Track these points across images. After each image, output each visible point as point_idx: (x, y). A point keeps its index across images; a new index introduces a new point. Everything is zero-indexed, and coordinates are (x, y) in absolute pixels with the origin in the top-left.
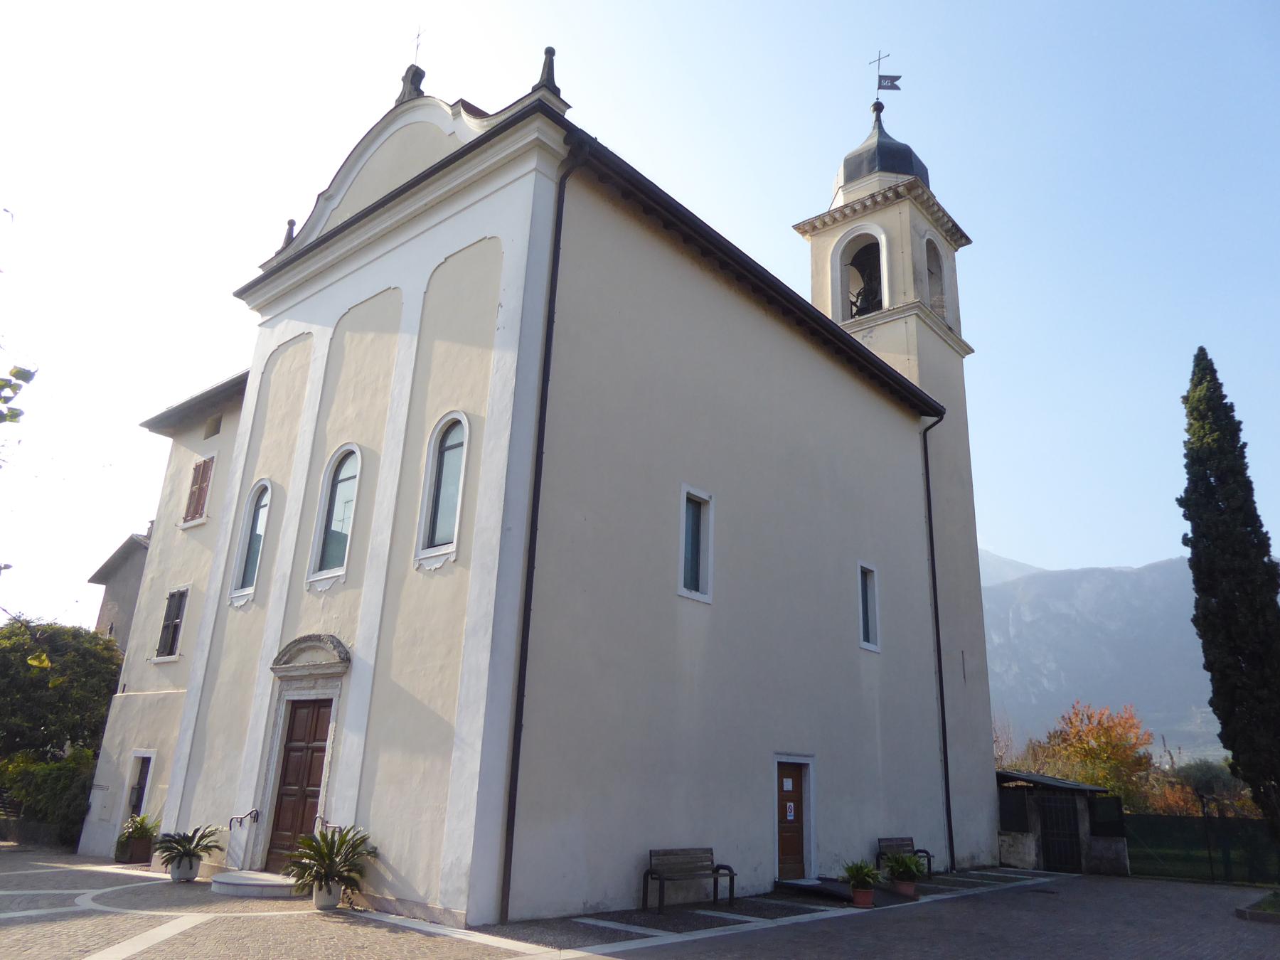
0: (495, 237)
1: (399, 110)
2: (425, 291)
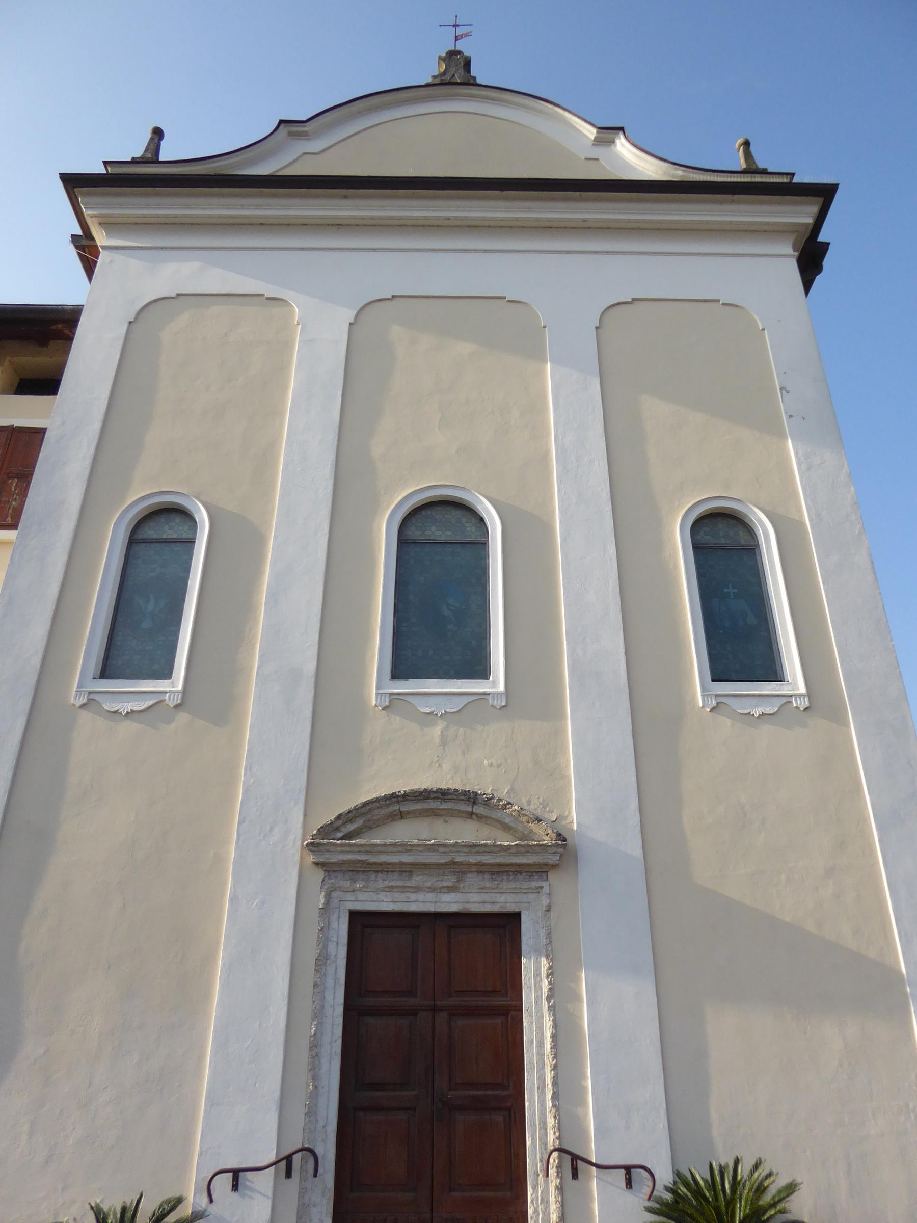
0: (741, 307)
1: (430, 90)
2: (352, 320)
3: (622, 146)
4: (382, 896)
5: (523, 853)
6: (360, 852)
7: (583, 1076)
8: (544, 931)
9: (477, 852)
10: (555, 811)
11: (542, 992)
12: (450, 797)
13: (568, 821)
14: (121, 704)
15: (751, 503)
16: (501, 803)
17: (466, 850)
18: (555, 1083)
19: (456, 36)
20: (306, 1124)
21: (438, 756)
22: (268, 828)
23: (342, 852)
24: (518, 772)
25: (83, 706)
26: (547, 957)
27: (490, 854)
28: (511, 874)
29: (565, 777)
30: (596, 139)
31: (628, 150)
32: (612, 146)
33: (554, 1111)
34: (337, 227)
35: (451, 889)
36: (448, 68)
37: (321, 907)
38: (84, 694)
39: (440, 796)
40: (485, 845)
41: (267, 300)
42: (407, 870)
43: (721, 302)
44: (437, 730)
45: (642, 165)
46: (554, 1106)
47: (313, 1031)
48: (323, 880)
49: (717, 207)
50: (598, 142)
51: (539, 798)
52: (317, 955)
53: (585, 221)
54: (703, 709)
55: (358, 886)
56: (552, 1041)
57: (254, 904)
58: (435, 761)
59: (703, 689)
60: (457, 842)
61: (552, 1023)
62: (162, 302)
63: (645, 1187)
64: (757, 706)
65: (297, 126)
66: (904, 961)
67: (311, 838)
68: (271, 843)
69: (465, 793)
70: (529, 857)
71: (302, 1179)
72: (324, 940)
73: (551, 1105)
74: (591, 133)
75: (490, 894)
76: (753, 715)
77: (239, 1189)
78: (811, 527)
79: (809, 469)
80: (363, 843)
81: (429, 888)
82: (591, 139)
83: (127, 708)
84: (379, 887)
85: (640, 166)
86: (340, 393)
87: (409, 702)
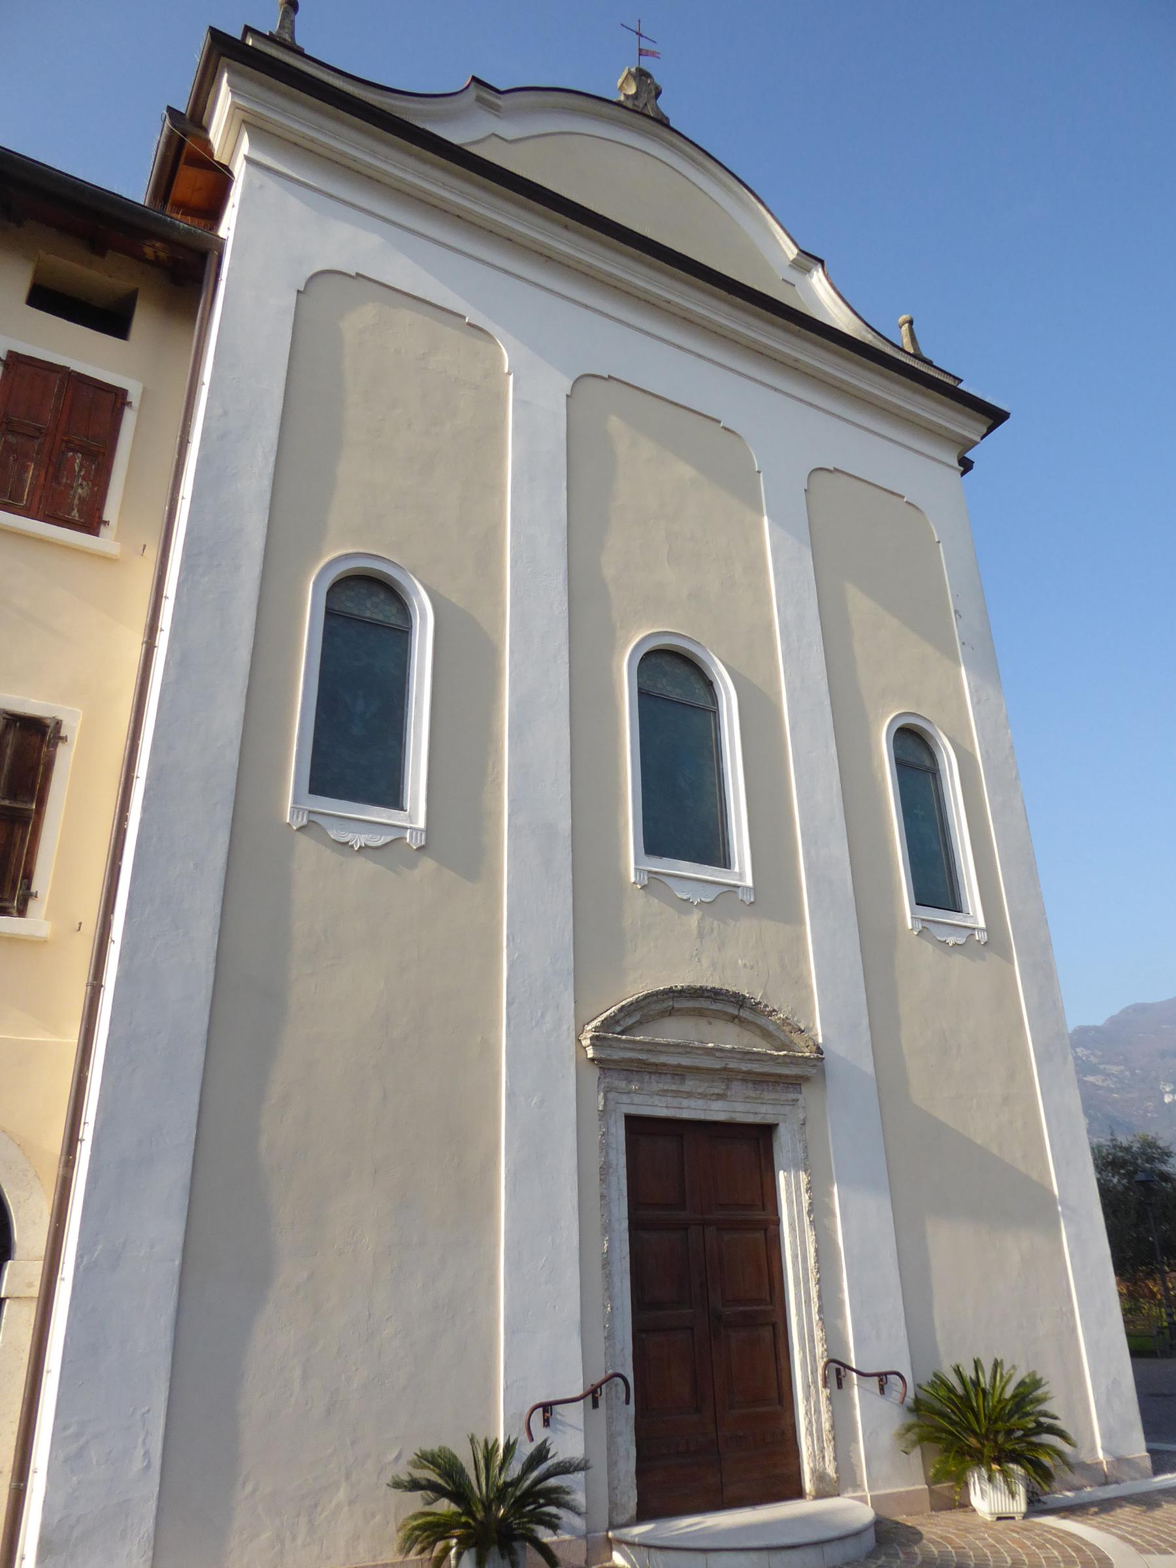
3: (818, 280)
4: (656, 1100)
5: (788, 1064)
6: (642, 1050)
7: (840, 1290)
8: (801, 1144)
9: (749, 1060)
10: (802, 1021)
11: (802, 1207)
12: (721, 997)
13: (813, 1033)
14: (350, 834)
15: (941, 730)
16: (767, 1009)
17: (739, 1056)
18: (820, 1297)
19: (639, 49)
20: (607, 1348)
21: (696, 949)
22: (539, 1015)
23: (625, 1049)
24: (769, 976)
25: (300, 829)
26: (806, 1171)
27: (759, 1062)
28: (770, 1084)
29: (808, 987)
30: (794, 261)
31: (825, 289)
32: (807, 275)
33: (820, 1324)
34: (544, 259)
35: (720, 1097)
36: (639, 90)
37: (600, 1109)
38: (303, 813)
39: (713, 996)
40: (758, 1053)
41: (468, 326)
42: (680, 1073)
43: (905, 500)
44: (694, 919)
45: (835, 312)
46: (820, 1319)
47: (605, 1247)
48: (599, 1078)
49: (909, 394)
50: (795, 264)
51: (788, 1006)
52: (602, 1163)
53: (796, 360)
54: (911, 932)
55: (634, 1087)
56: (816, 1256)
57: (534, 1102)
58: (694, 954)
59: (296, 800)
60: (734, 1048)
61: (814, 1237)
62: (338, 277)
63: (894, 1393)
64: (950, 935)
65: (489, 93)
66: (1057, 1182)
67: (593, 1030)
68: (544, 1032)
69: (735, 995)
70: (792, 1069)
71: (609, 1408)
72: (605, 1147)
73: (818, 1318)
74: (792, 252)
75: (753, 1104)
76: (948, 943)
77: (885, 1392)
78: (983, 761)
79: (979, 702)
80: (647, 1040)
81: (700, 1094)
82: (789, 258)
83: (360, 840)
84: (653, 1090)
85: (833, 312)
86: (565, 484)
87: (666, 884)
